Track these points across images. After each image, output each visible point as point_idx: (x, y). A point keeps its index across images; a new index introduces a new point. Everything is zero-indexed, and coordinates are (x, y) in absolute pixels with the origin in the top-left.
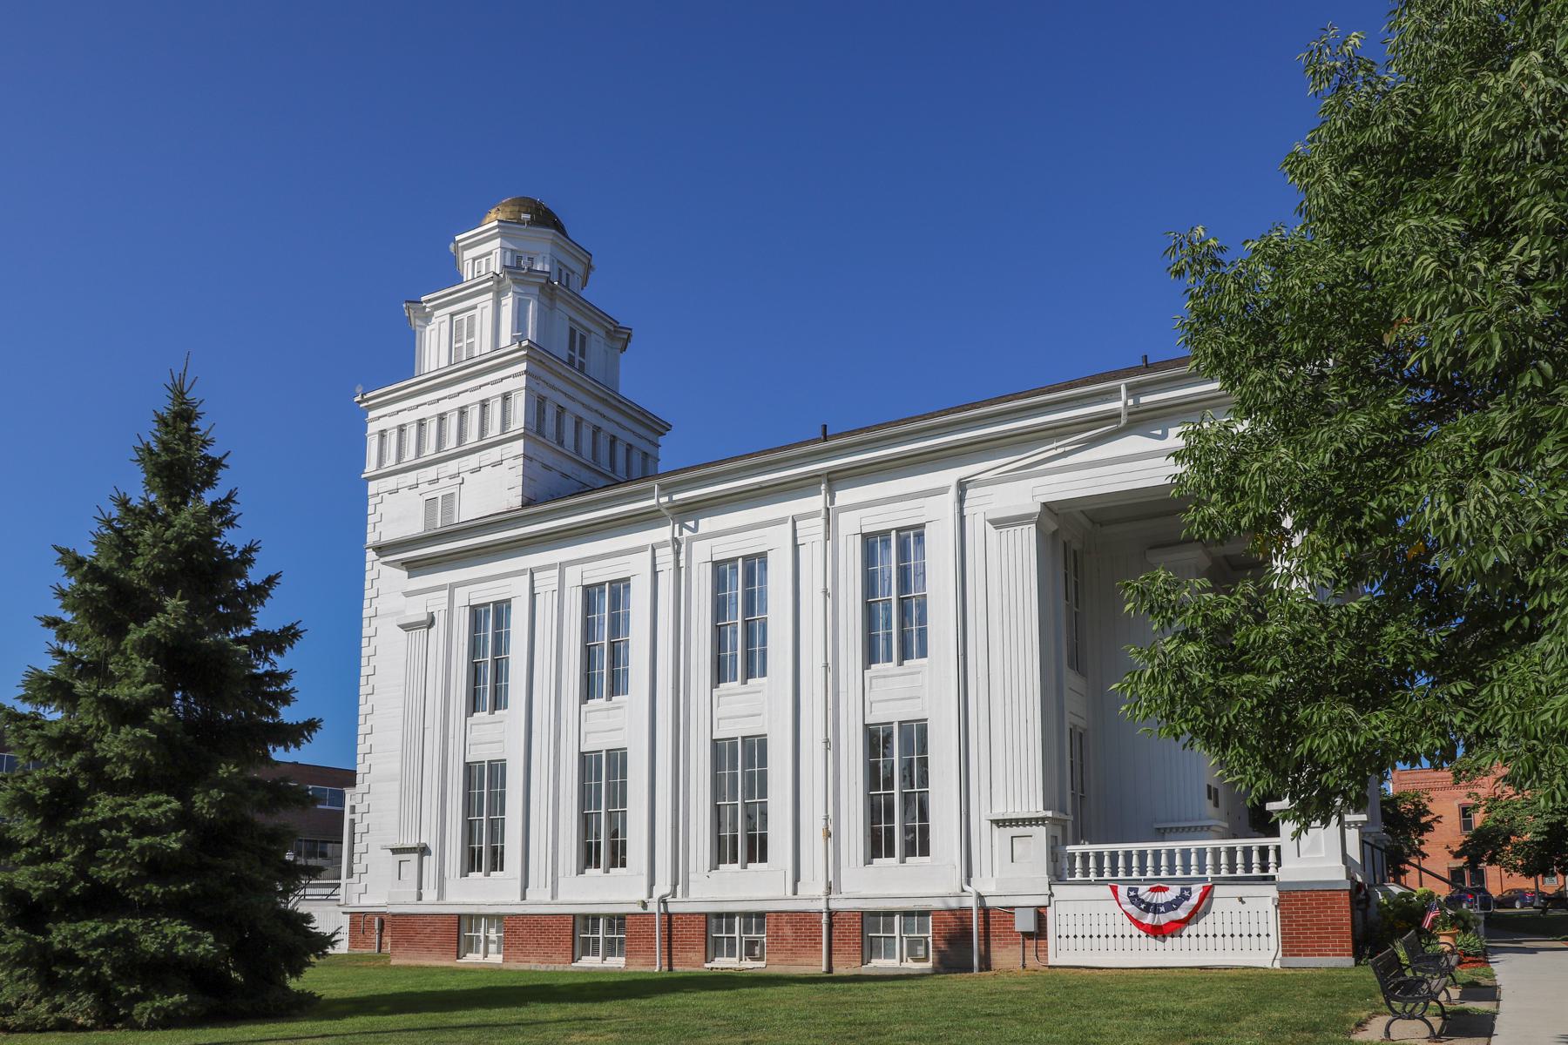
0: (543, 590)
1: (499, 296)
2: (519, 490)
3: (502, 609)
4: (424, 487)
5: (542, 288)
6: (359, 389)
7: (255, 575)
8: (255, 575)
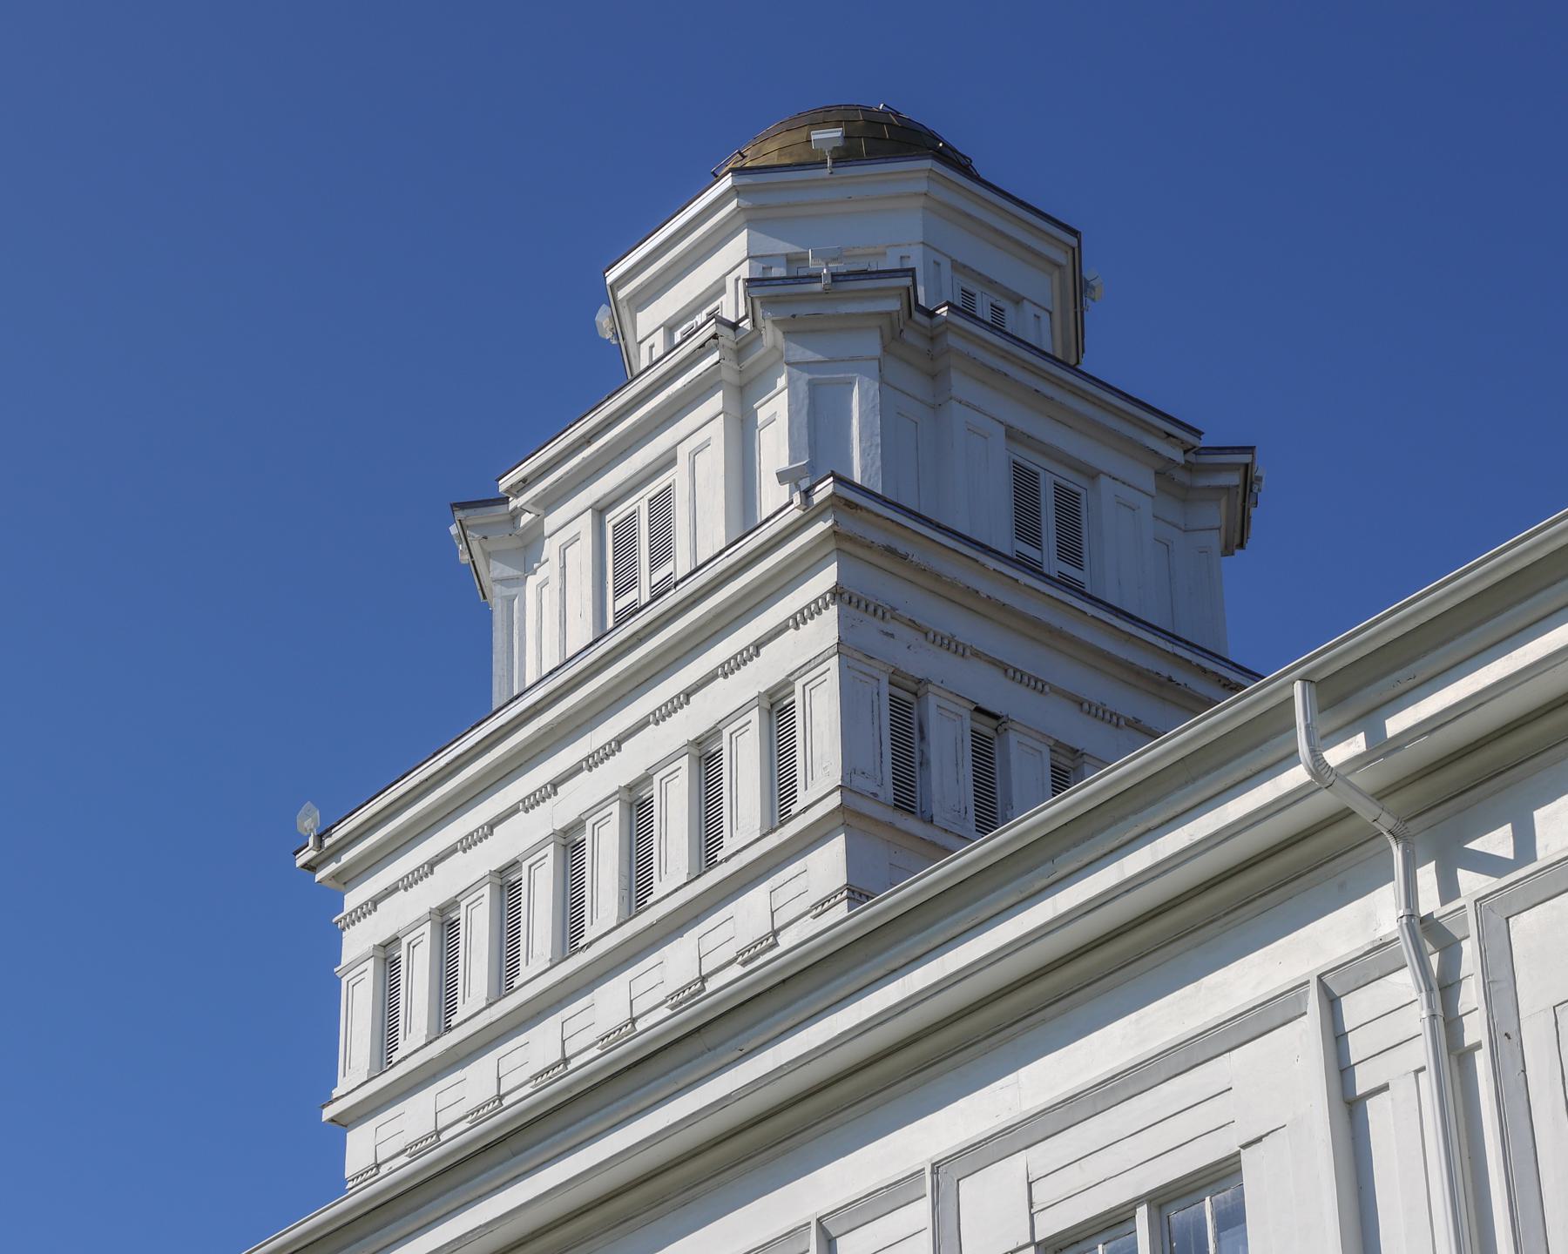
1: (744, 396)
5: (893, 334)
6: (308, 822)
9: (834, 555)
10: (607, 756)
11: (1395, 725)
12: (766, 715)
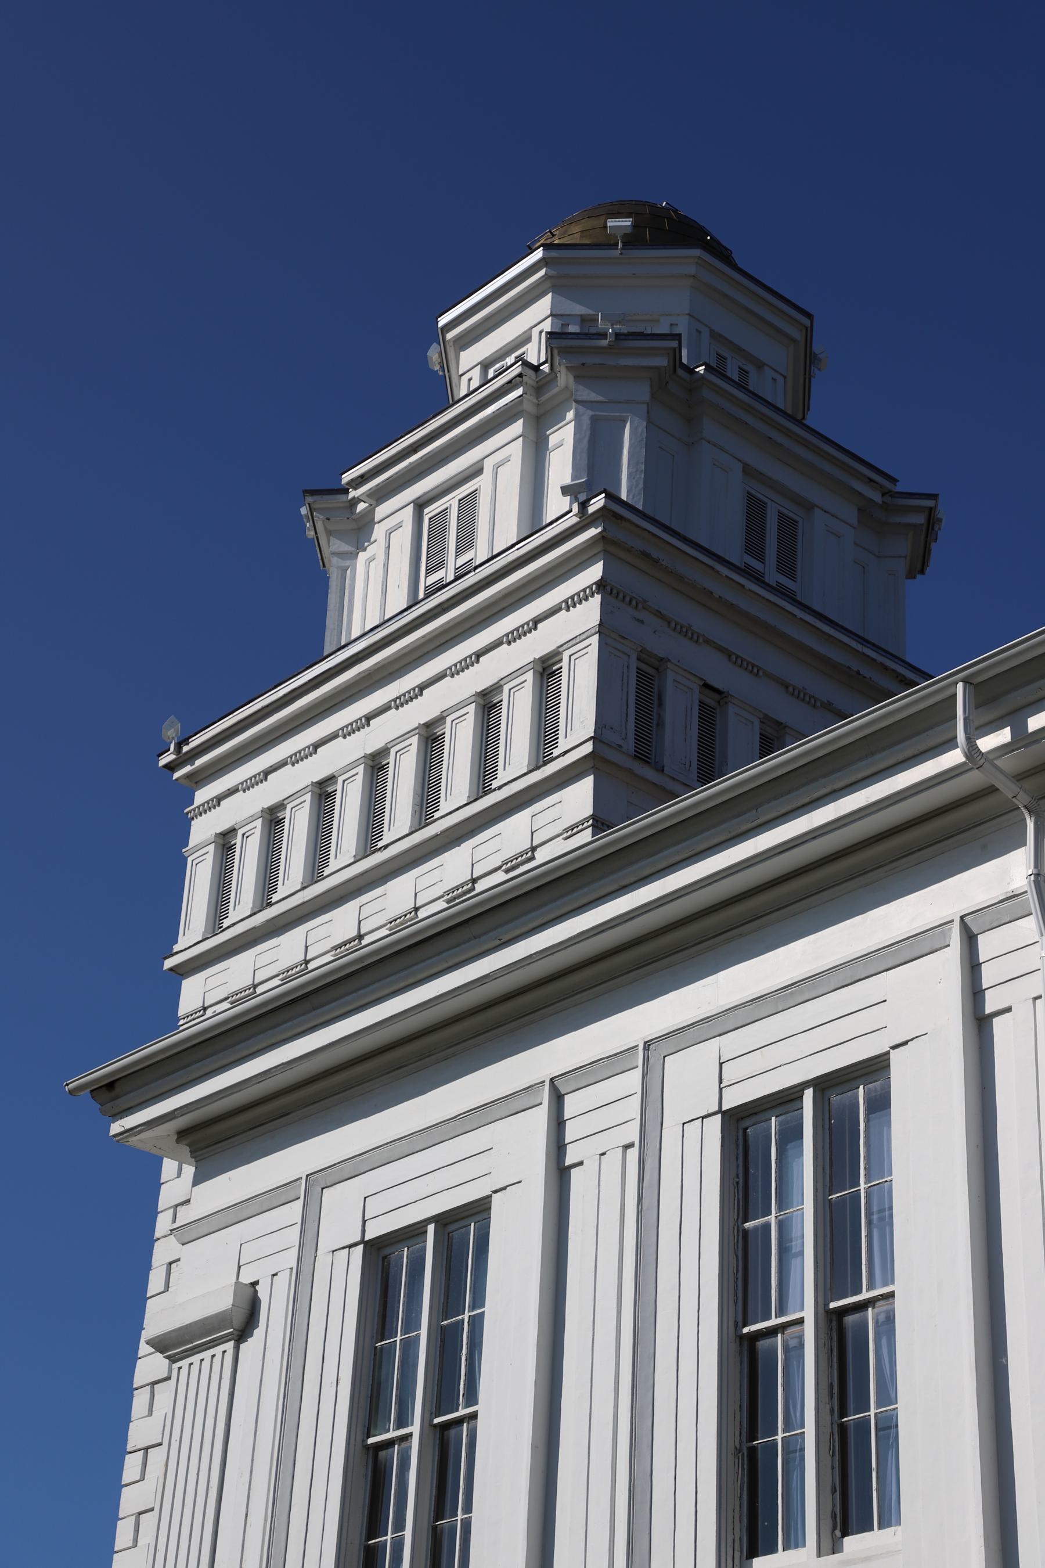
6: (171, 732)
9: (601, 555)
10: (411, 699)
12: (538, 676)
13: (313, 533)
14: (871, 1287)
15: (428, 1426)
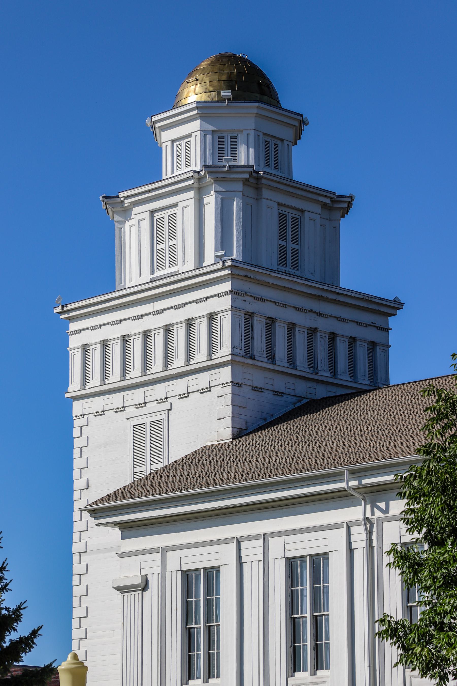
0: (249, 555)
1: (200, 192)
2: (228, 421)
3: (212, 575)
4: (131, 411)
5: (245, 182)
7: (22, 630)
8: (22, 630)
9: (230, 279)
10: (159, 313)
11: (365, 481)
12: (208, 319)
13: (105, 207)
14: (324, 611)
15: (205, 626)
